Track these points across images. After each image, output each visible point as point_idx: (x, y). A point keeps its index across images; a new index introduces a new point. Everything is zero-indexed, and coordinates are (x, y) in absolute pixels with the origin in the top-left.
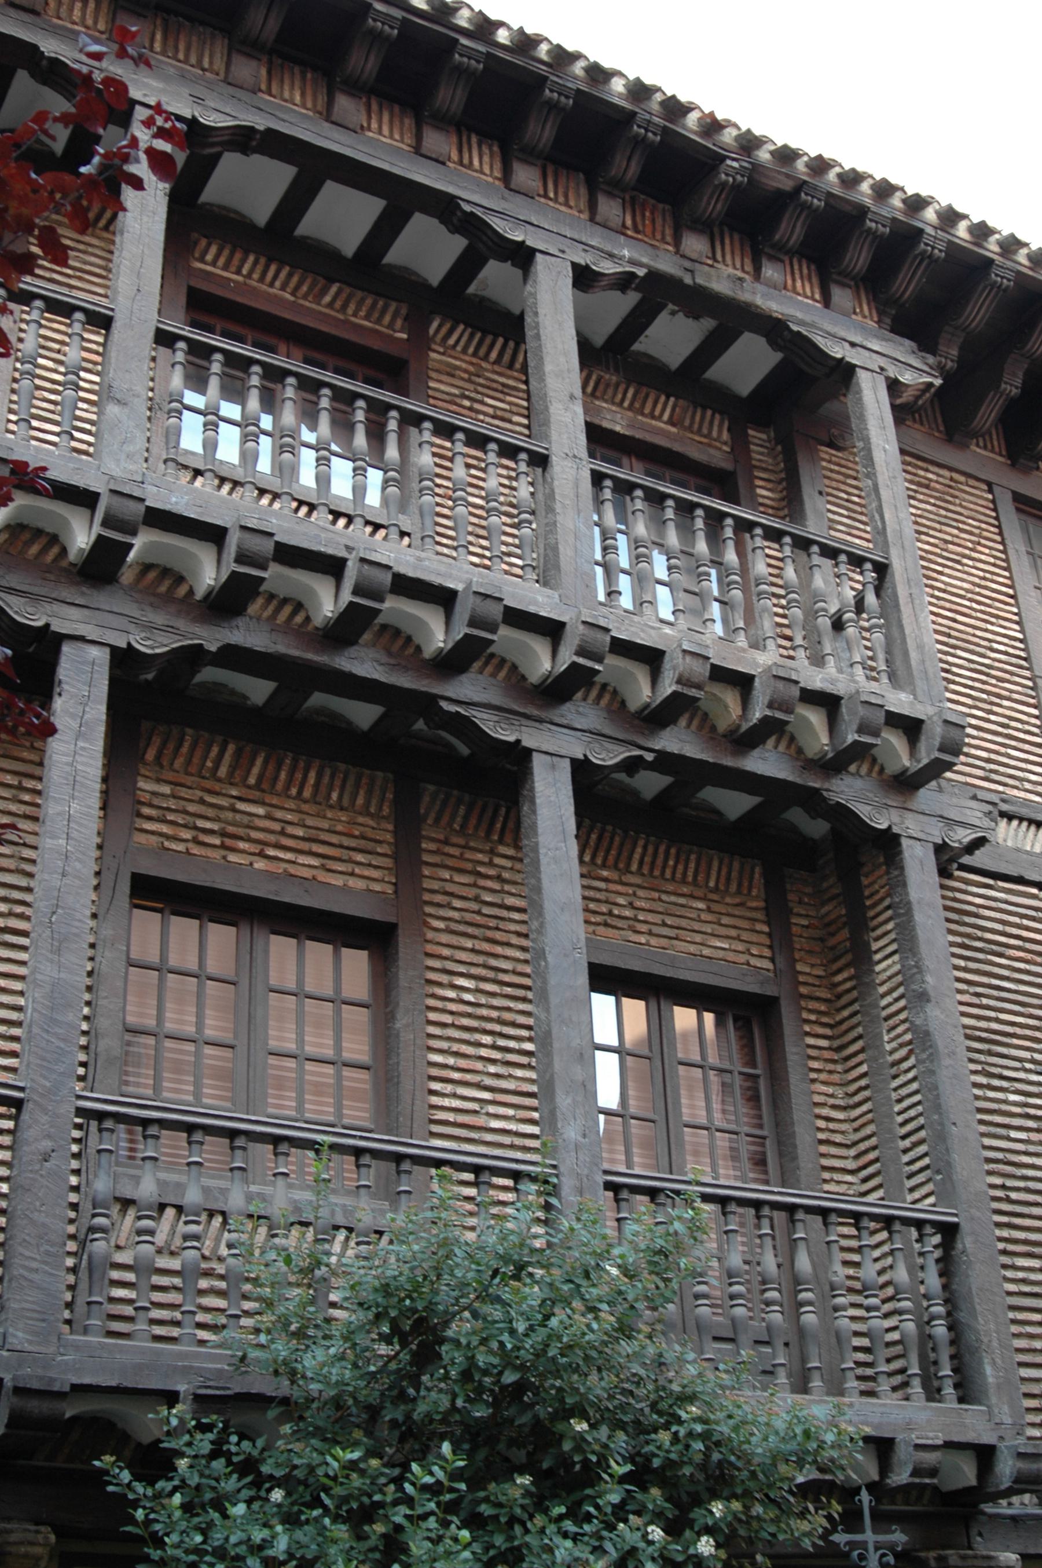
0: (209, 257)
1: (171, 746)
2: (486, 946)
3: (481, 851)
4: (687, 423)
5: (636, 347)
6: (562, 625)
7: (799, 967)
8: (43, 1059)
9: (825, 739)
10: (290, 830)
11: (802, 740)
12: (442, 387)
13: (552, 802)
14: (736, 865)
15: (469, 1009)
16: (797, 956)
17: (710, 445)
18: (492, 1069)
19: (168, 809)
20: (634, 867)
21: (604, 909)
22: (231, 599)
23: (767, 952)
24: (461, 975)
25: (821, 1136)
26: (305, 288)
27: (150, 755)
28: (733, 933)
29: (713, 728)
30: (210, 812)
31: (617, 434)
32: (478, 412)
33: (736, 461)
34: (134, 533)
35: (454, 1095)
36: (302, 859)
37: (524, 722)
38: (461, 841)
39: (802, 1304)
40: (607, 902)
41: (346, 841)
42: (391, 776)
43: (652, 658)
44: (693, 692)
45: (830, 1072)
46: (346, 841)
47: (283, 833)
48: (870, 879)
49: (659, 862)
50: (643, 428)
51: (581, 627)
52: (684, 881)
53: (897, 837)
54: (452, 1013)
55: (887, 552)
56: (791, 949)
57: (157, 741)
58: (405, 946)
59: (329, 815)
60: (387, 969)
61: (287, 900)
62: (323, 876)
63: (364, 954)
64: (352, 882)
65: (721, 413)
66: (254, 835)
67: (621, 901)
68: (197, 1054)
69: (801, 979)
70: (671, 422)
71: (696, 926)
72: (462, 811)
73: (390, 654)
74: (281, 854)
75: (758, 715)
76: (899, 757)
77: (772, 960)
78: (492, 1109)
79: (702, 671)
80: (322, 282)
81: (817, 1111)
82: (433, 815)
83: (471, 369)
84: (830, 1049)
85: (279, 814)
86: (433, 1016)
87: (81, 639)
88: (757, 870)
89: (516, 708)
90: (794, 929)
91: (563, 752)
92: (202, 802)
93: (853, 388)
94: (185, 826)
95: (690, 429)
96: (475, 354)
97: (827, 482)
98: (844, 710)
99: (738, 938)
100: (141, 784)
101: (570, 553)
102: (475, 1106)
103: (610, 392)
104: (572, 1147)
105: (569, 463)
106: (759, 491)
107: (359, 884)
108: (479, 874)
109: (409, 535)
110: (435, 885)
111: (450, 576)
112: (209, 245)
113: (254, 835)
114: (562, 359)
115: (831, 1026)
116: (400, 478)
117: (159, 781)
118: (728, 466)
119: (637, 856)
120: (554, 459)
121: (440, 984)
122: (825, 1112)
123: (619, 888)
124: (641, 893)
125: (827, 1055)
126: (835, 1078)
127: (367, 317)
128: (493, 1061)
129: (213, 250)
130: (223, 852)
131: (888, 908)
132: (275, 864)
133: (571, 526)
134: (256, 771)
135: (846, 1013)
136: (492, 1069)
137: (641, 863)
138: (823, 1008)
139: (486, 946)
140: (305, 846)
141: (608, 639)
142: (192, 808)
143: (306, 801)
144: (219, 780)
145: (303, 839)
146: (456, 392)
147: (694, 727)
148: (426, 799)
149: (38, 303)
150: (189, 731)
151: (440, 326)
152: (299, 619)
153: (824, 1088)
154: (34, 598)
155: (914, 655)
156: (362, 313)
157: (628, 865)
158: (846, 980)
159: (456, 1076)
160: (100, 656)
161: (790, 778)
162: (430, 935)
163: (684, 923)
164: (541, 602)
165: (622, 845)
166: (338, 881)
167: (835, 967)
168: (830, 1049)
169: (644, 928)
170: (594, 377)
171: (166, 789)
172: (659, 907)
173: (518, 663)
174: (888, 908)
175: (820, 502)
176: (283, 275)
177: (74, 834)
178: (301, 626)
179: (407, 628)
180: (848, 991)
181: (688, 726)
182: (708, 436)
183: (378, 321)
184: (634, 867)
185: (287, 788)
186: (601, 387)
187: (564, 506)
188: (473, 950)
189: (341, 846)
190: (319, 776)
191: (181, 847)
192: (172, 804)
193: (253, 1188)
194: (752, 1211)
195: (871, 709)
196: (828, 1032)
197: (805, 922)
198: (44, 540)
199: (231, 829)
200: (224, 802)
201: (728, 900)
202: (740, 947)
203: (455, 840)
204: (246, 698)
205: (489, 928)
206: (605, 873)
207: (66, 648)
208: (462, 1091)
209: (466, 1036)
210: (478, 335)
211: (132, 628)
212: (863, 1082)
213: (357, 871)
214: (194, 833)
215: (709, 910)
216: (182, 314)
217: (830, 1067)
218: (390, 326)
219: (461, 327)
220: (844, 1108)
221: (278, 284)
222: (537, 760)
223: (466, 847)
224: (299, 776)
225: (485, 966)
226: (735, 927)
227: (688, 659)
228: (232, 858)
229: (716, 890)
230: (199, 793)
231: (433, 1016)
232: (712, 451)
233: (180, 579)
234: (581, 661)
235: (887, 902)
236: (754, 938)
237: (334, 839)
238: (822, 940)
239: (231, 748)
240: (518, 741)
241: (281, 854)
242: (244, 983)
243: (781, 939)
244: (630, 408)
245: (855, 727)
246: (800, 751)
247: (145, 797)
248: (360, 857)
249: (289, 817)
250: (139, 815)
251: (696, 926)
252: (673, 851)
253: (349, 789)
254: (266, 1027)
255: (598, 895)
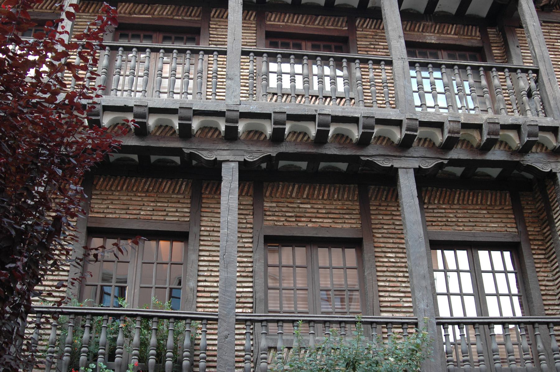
0: (272, 19)
1: (275, 190)
2: (398, 241)
3: (394, 206)
4: (462, 32)
5: (437, 10)
6: (401, 121)
7: (528, 229)
8: (224, 304)
9: (518, 142)
10: (320, 211)
11: (510, 144)
12: (363, 43)
13: (407, 185)
14: (498, 194)
15: (393, 264)
16: (527, 225)
17: (472, 39)
18: (404, 285)
19: (276, 211)
20: (456, 202)
21: (444, 219)
22: (278, 137)
23: (514, 225)
24: (389, 252)
25: (543, 293)
26: (308, 21)
27: (268, 194)
28: (499, 220)
29: (472, 146)
30: (291, 210)
31: (433, 43)
32: (378, 48)
33: (483, 42)
34: (237, 122)
35: (390, 296)
36: (325, 221)
37: (394, 158)
38: (386, 204)
39: (541, 361)
40: (445, 217)
41: (341, 211)
42: (357, 185)
43: (439, 125)
44: (456, 135)
45: (546, 267)
46: (341, 211)
47: (318, 212)
48: (550, 191)
49: (466, 198)
50: (444, 39)
51: (406, 120)
52: (477, 204)
53: (555, 173)
54: (387, 267)
55: (538, 65)
56: (525, 223)
57: (270, 189)
58: (366, 245)
59: (334, 203)
60: (362, 254)
61: (320, 236)
62: (333, 225)
63: (354, 250)
64: (345, 226)
65: (475, 26)
66: (307, 215)
67: (451, 215)
68: (294, 294)
69: (530, 233)
70: (455, 34)
71: (483, 220)
72: (385, 193)
73: (340, 144)
74: (318, 220)
75: (485, 138)
76: (551, 142)
77: (517, 228)
78: (404, 299)
79: (458, 126)
80: (314, 17)
81: (541, 283)
82: (374, 197)
83: (373, 34)
84: (545, 258)
85: (316, 206)
86: (379, 269)
87: (228, 161)
88: (508, 194)
89: (390, 154)
90: (525, 215)
91: (410, 166)
92: (287, 207)
93: (519, 5)
94: (282, 216)
95: (463, 34)
96: (374, 28)
97: (520, 42)
98: (522, 129)
99: (501, 222)
100: (265, 204)
101: (402, 94)
102: (398, 299)
103: (429, 29)
104: (423, 311)
105: (400, 61)
106: (494, 51)
107: (348, 226)
108: (393, 215)
109: (354, 99)
110: (377, 222)
111: (356, 112)
112: (272, 15)
113: (307, 215)
114: (395, 24)
115: (545, 250)
116: (348, 80)
117: (272, 202)
118: (480, 45)
119: (456, 198)
120: (394, 61)
121: (381, 257)
122: (544, 283)
123: (450, 211)
124: (459, 211)
125: (543, 261)
126: (548, 269)
127: (332, 25)
128: (404, 282)
129: (274, 16)
130: (297, 223)
131: (557, 201)
132: (316, 223)
133: (402, 84)
134: (306, 193)
135: (549, 244)
136: (404, 285)
137: (458, 200)
138: (540, 243)
139: (398, 241)
140: (326, 216)
141: (418, 123)
142: (284, 209)
143: (326, 200)
144: (293, 198)
145: (325, 213)
146: (368, 43)
147: (463, 148)
148: (371, 191)
149: (201, 52)
150: (281, 183)
151: (360, 21)
152: (305, 138)
153: (543, 274)
154: (210, 150)
155: (552, 102)
156: (330, 24)
157: (453, 201)
158: (547, 231)
159: (390, 289)
160: (235, 165)
161: (506, 159)
162: (376, 240)
163: (478, 220)
164: (393, 114)
165: (450, 195)
166: (339, 226)
167: (543, 227)
168: (545, 258)
169: (461, 224)
170: (422, 25)
171: (274, 205)
172: (467, 215)
173: (390, 137)
174: (557, 201)
175: (518, 50)
176: (299, 18)
177: (230, 227)
178: (306, 141)
179: (346, 134)
180: (549, 235)
181: (462, 147)
182: (471, 35)
183: (337, 25)
184: (456, 202)
185: (318, 196)
186: (425, 28)
187: (399, 77)
188: (393, 243)
189: (340, 214)
190: (330, 190)
191: (281, 224)
192: (277, 209)
193: (317, 338)
194: (531, 326)
195: (532, 127)
196: (543, 252)
197: (530, 211)
198: (213, 131)
199: (298, 214)
200: (295, 205)
201: (496, 208)
202: (503, 225)
203: (383, 204)
204: (301, 168)
205: (399, 234)
206: (444, 206)
207: (223, 165)
208: (392, 294)
209: (392, 274)
210: (375, 21)
211: (245, 154)
212: (557, 270)
213: (346, 221)
214: (286, 218)
215: (488, 213)
216: (264, 41)
217: (546, 265)
218: (341, 26)
219: (368, 20)
220: (553, 281)
221: (298, 22)
222: (400, 172)
223: (388, 206)
224: (322, 191)
225: (398, 248)
226: (500, 218)
227: (451, 123)
228: (300, 224)
229: (491, 205)
230: (286, 204)
231: (379, 269)
232: (473, 41)
233: (262, 133)
234: (408, 133)
235: (556, 199)
236: (508, 220)
237: (337, 211)
238: (538, 217)
239: (296, 186)
240: (392, 166)
241: (318, 220)
242: (310, 267)
243: (520, 220)
244: (438, 32)
245: (526, 135)
246: (510, 148)
247: (267, 209)
248: (347, 216)
249: (319, 207)
250: (266, 215)
251: (483, 220)
252: (471, 193)
253: (341, 192)
254: (319, 281)
255: (442, 215)
